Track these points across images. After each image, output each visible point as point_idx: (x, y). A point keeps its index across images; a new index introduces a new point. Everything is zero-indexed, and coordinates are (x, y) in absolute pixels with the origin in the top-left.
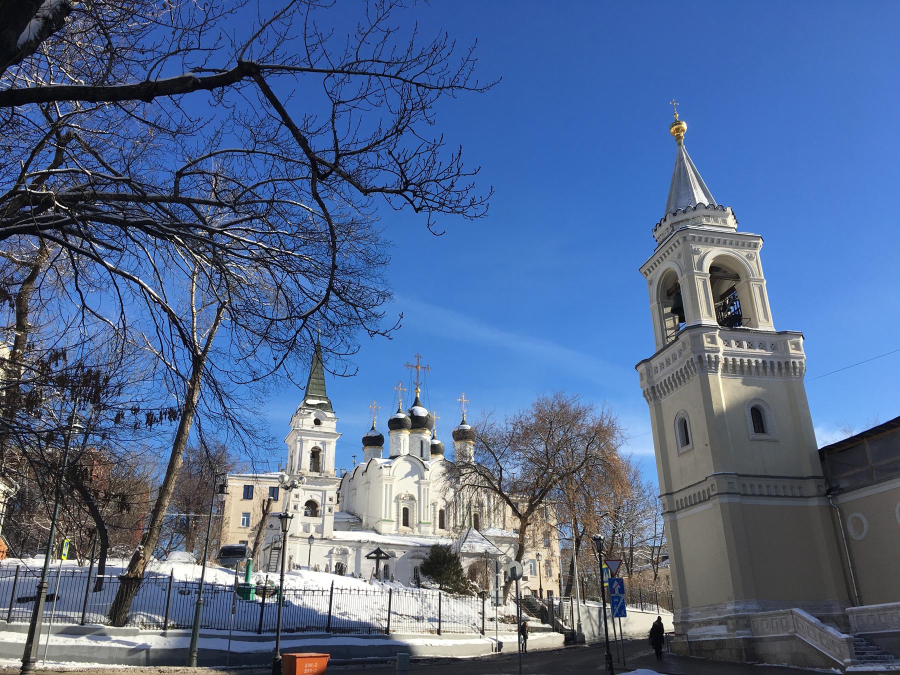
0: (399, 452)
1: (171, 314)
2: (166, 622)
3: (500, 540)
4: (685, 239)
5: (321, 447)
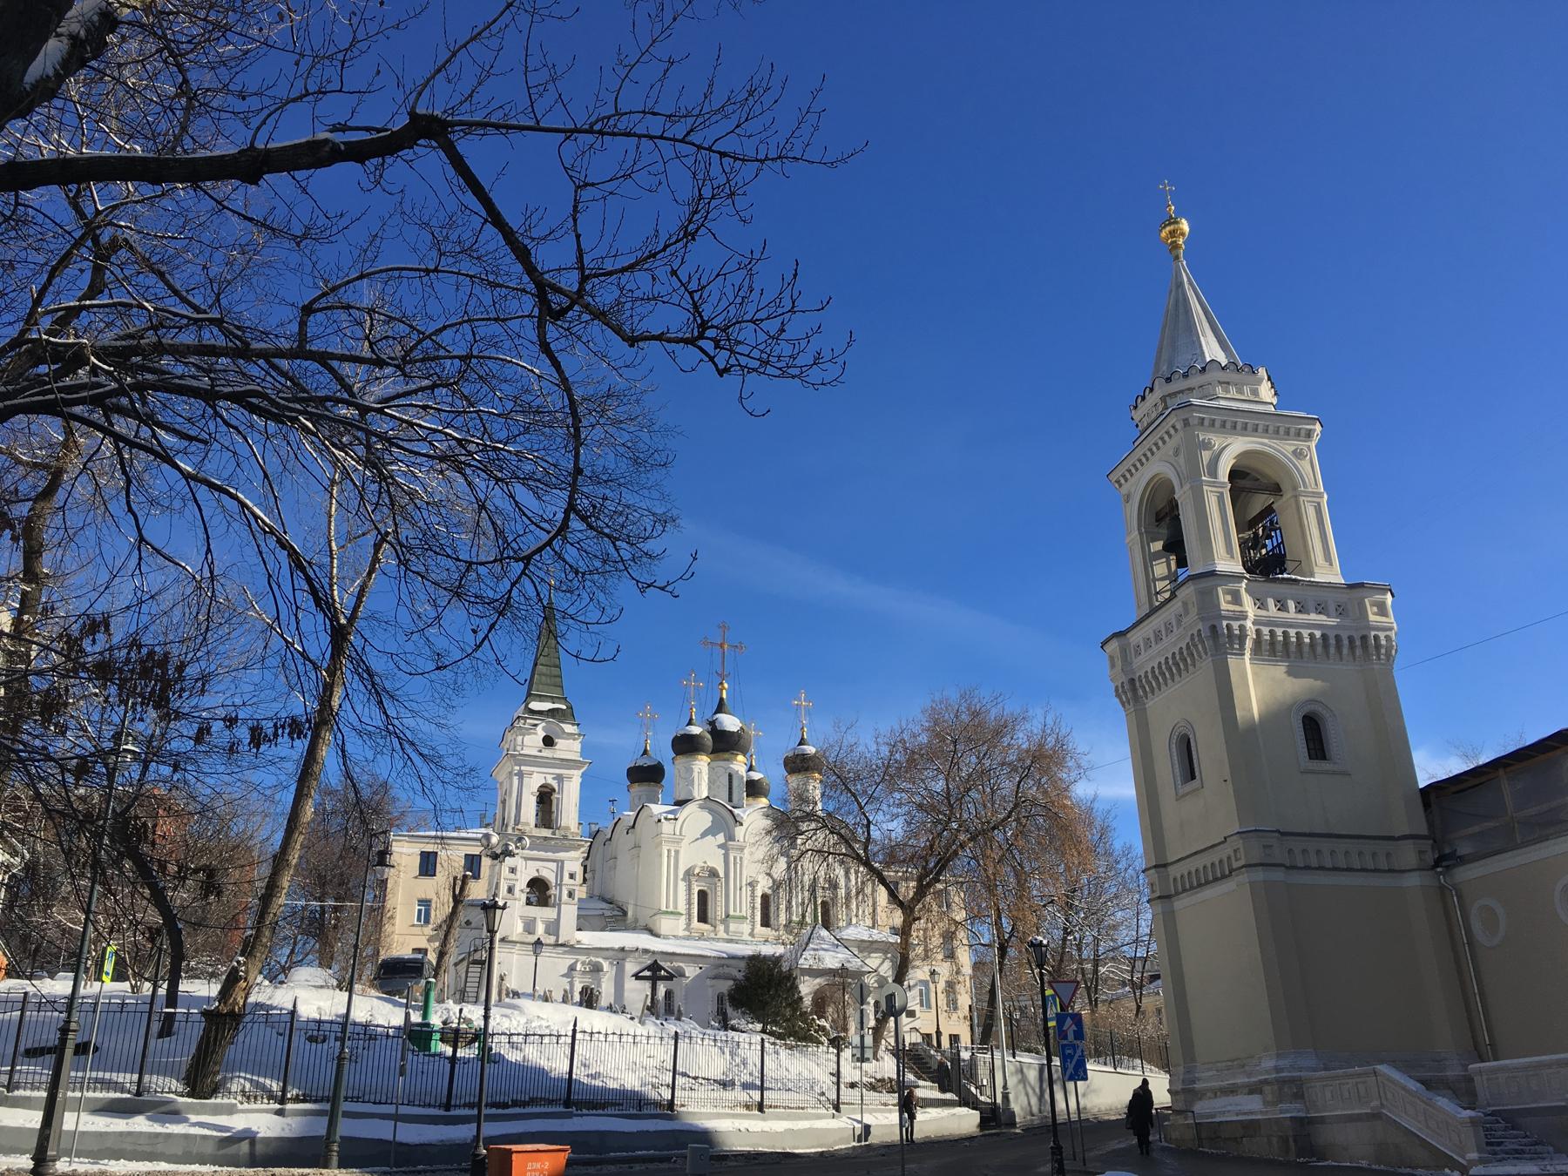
0: (691, 792)
1: (292, 553)
2: (284, 1090)
3: (867, 947)
4: (1186, 423)
5: (555, 784)
